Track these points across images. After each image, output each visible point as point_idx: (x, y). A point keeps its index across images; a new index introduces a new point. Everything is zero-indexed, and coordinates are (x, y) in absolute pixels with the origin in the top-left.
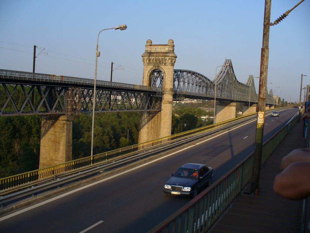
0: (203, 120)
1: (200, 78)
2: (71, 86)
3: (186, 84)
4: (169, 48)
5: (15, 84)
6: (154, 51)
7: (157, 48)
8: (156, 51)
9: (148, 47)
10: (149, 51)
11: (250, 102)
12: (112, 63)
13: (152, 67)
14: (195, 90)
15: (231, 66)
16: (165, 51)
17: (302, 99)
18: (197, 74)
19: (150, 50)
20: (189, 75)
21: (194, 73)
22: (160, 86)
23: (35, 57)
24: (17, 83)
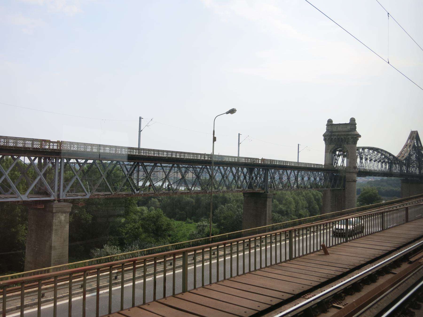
0: (105, 245)
1: (382, 154)
2: (208, 164)
3: (364, 160)
4: (351, 126)
5: (171, 164)
6: (335, 130)
7: (339, 127)
8: (337, 131)
9: (329, 126)
10: (331, 130)
11: (9, 190)
12: (299, 145)
13: (333, 146)
14: (376, 166)
15: (418, 138)
16: (347, 130)
17: (300, 247)
18: (384, 151)
19: (331, 129)
20: (371, 151)
21: (374, 149)
22: (342, 164)
23: (140, 131)
24: (202, 165)
